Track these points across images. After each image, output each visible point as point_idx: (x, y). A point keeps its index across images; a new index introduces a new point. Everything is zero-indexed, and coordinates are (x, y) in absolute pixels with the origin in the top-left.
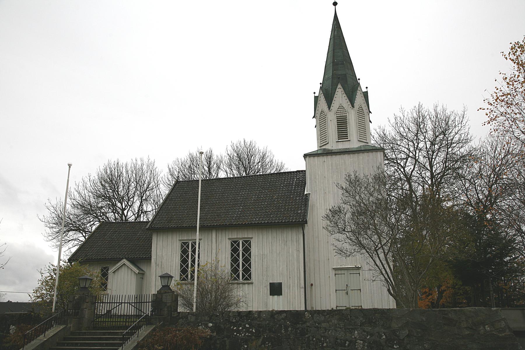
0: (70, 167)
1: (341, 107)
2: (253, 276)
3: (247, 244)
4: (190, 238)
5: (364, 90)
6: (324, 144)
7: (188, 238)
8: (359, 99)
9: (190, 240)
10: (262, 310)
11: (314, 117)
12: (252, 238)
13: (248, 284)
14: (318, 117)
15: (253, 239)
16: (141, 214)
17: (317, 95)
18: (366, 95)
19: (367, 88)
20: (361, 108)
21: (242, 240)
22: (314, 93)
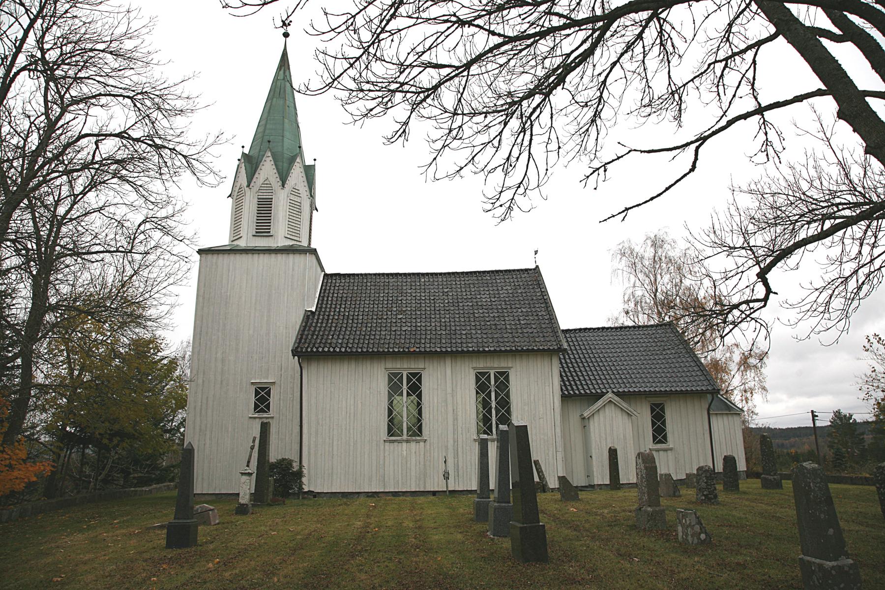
0: (246, 4)
1: (267, 185)
2: (670, 437)
3: (503, 380)
4: (405, 366)
5: (309, 162)
6: (291, 237)
7: (409, 366)
8: (296, 176)
9: (492, 368)
10: (437, 490)
11: (230, 196)
12: (510, 368)
13: (665, 450)
14: (235, 198)
15: (512, 369)
16: (777, 251)
17: (246, 151)
18: (309, 172)
19: (315, 160)
20: (295, 192)
21: (493, 371)
22: (243, 147)
